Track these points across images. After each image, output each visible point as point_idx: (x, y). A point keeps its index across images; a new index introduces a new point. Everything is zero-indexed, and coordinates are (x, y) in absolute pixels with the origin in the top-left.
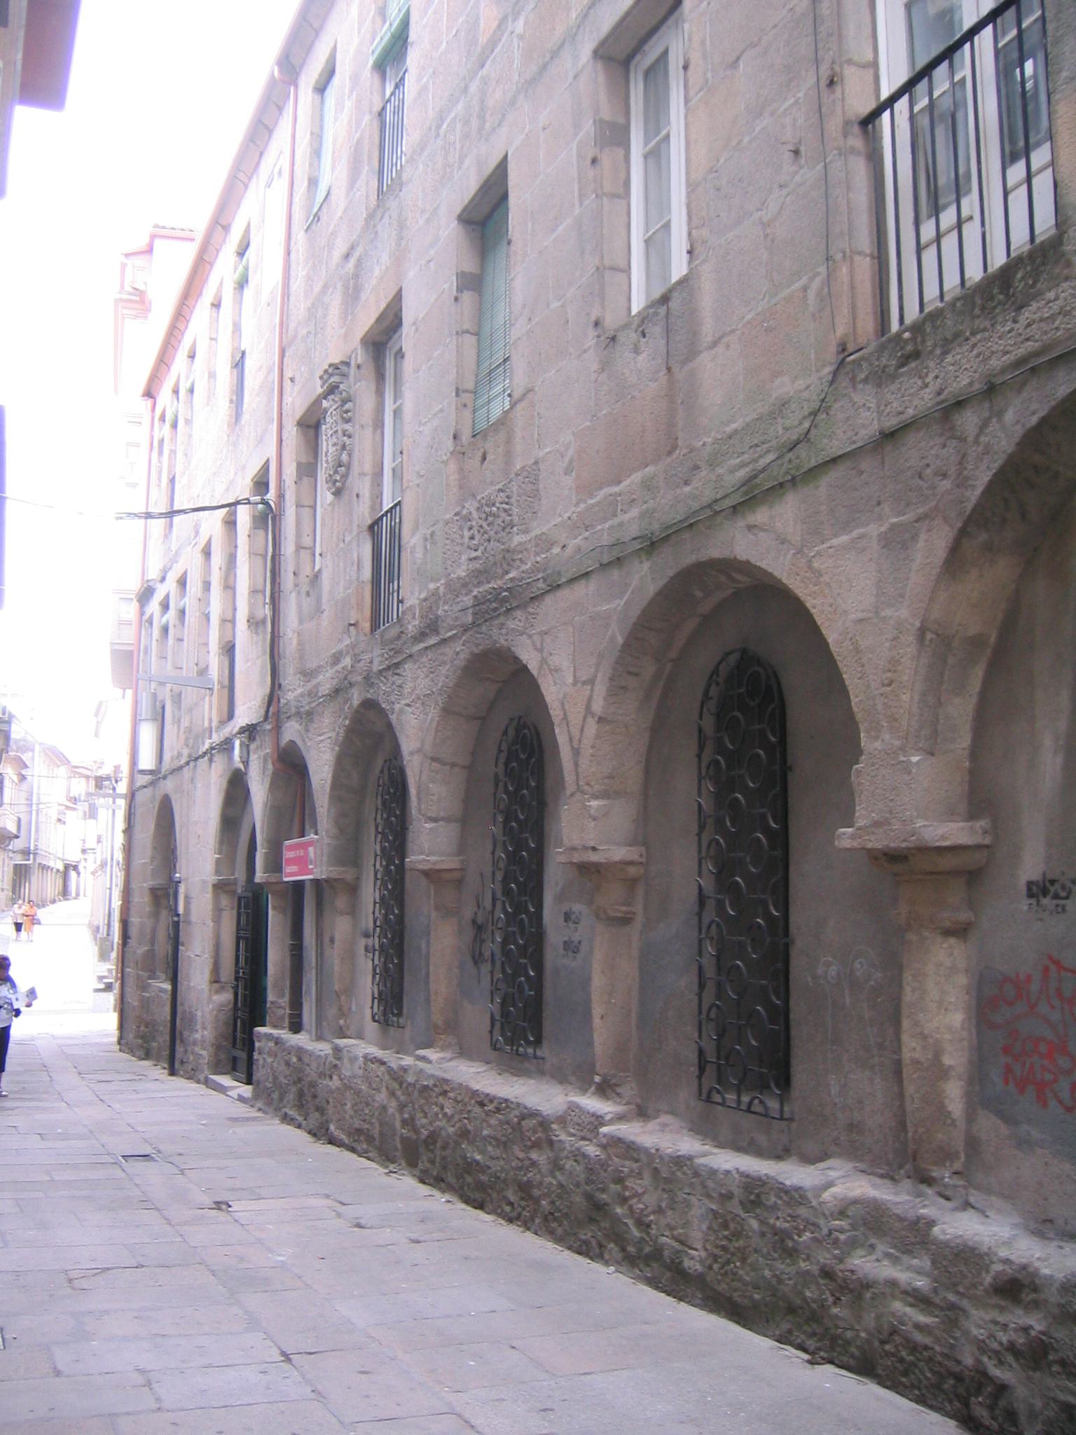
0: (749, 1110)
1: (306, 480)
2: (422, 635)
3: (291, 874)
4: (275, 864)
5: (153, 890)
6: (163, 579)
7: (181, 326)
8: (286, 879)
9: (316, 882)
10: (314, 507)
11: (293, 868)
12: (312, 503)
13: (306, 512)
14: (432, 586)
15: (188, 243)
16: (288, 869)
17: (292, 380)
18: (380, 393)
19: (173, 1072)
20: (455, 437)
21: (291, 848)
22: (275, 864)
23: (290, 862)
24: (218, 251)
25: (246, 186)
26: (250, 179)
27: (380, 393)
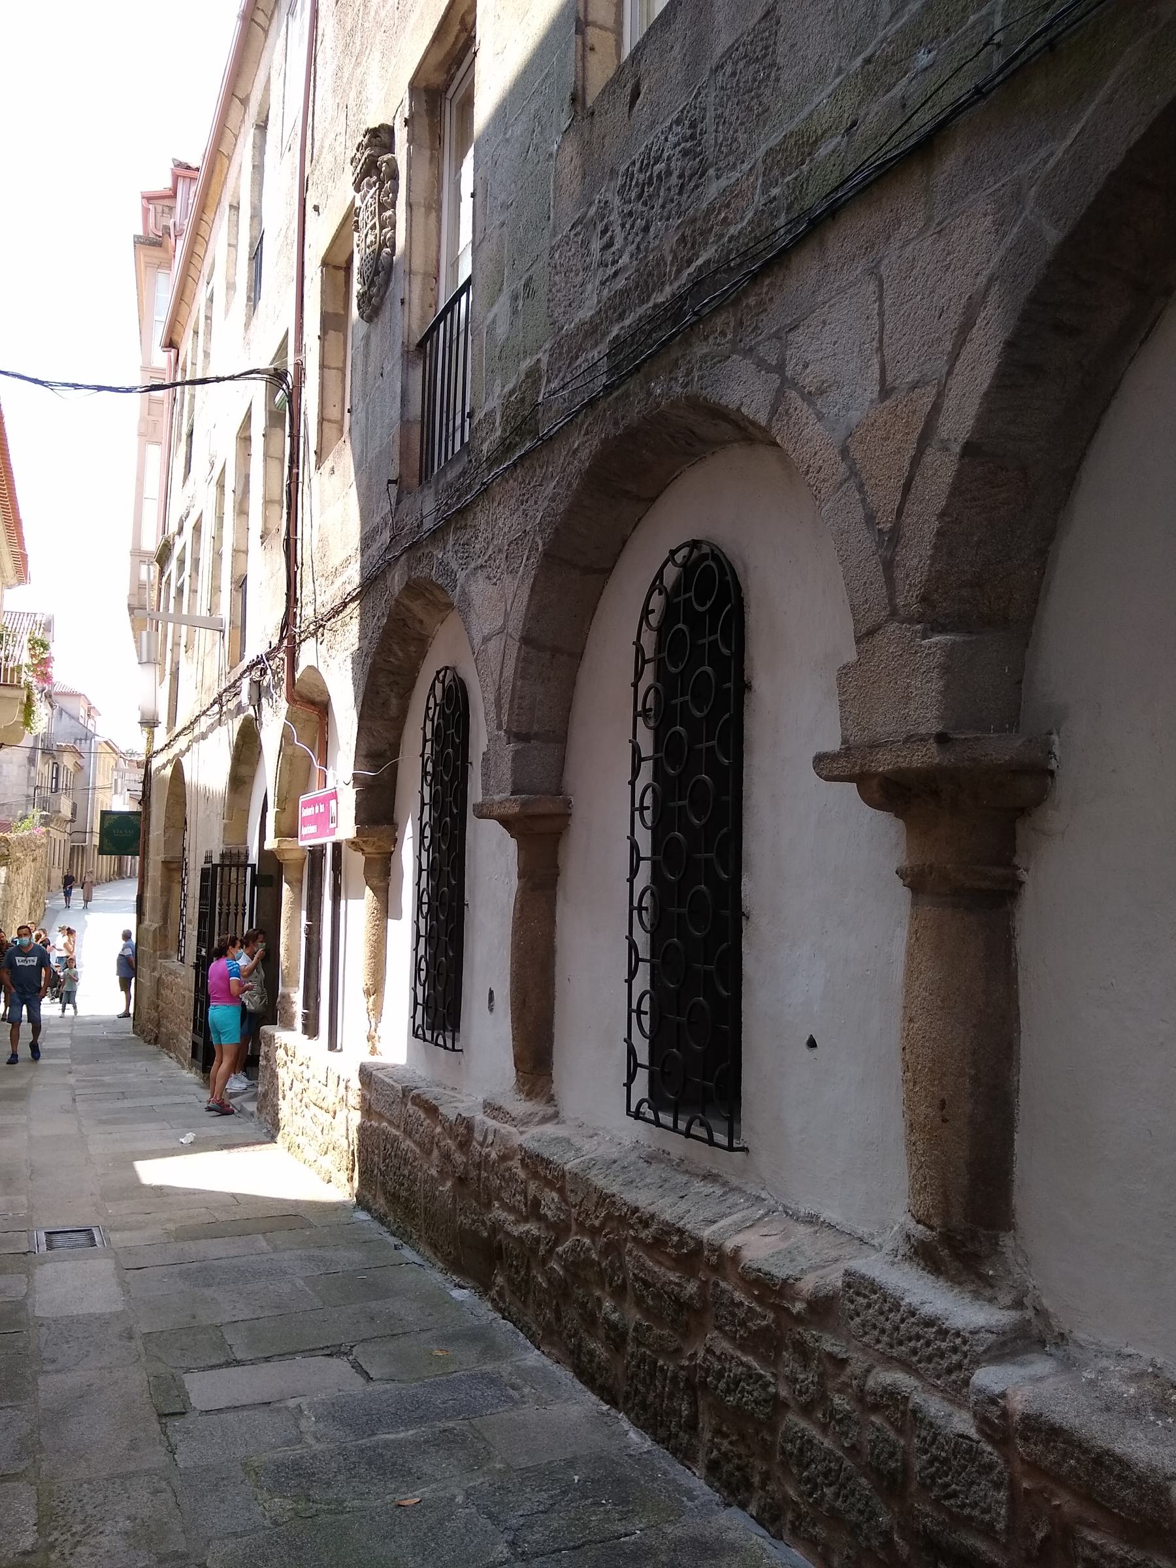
0: (688, 1134)
1: (331, 333)
2: (506, 447)
3: (308, 837)
4: (288, 831)
5: (165, 863)
6: (180, 531)
7: (199, 250)
8: (301, 843)
9: (337, 846)
10: (343, 370)
11: (312, 829)
12: (340, 365)
13: (332, 375)
14: (526, 364)
15: (361, 1380)
16: (305, 830)
17: (316, 208)
18: (409, 326)
19: (858, 640)
20: (574, 99)
21: (308, 804)
22: (288, 831)
23: (308, 821)
24: (236, 137)
25: (266, 32)
26: (270, 20)
27: (409, 326)
